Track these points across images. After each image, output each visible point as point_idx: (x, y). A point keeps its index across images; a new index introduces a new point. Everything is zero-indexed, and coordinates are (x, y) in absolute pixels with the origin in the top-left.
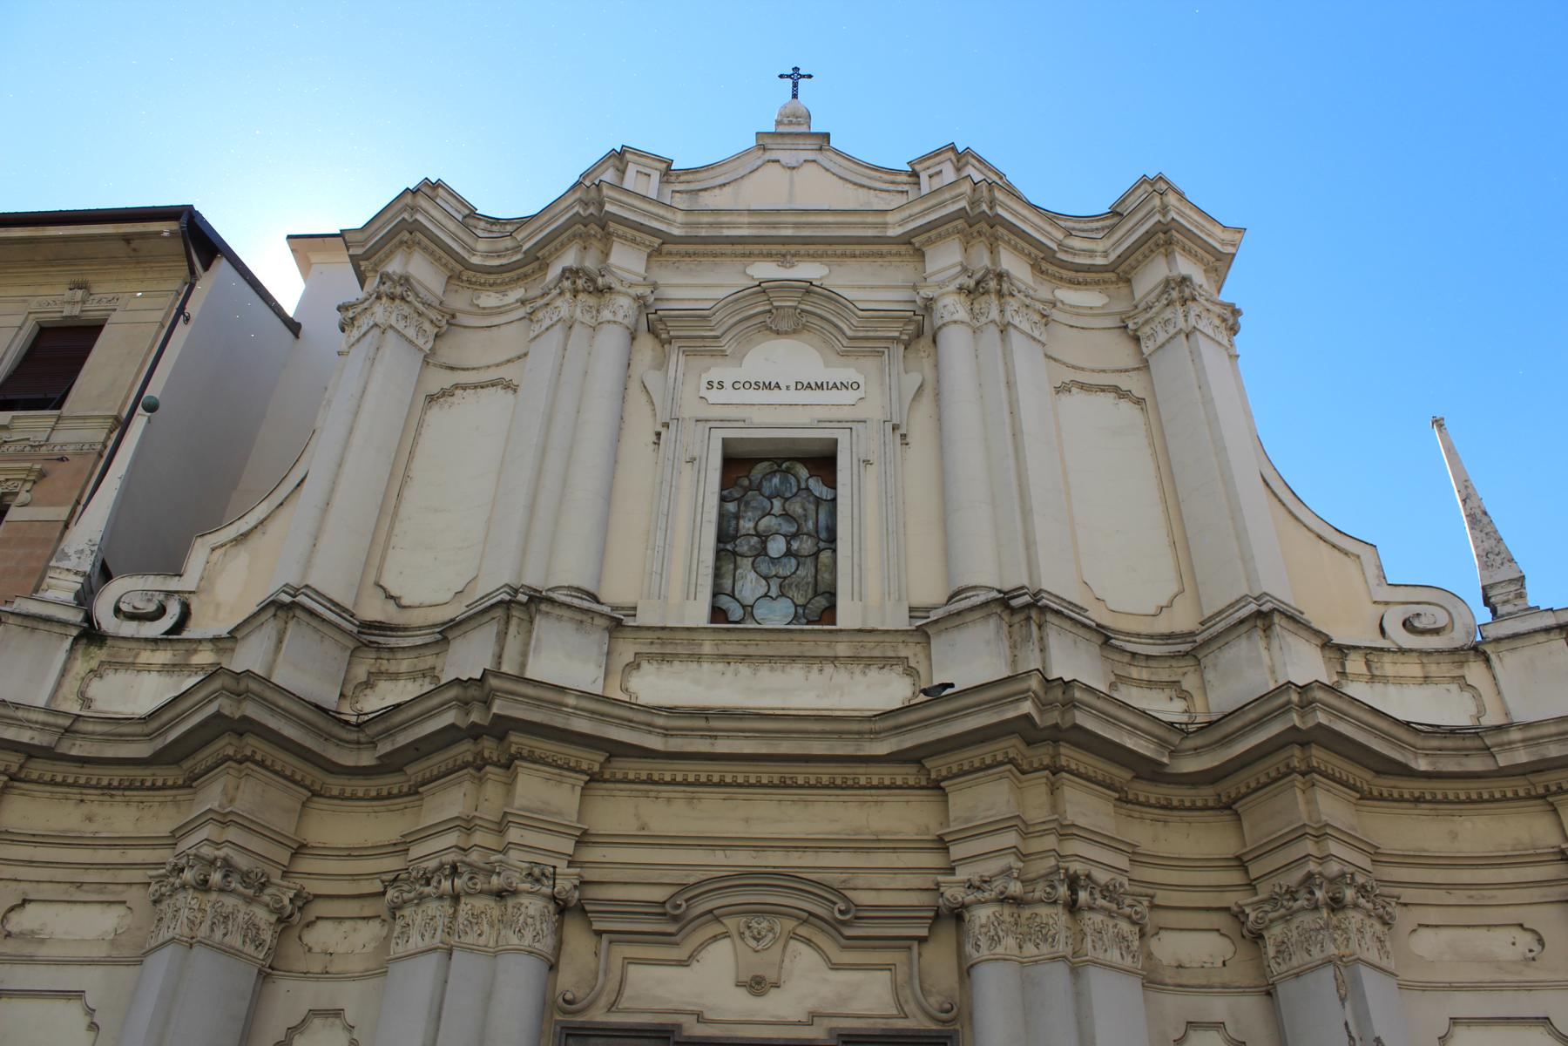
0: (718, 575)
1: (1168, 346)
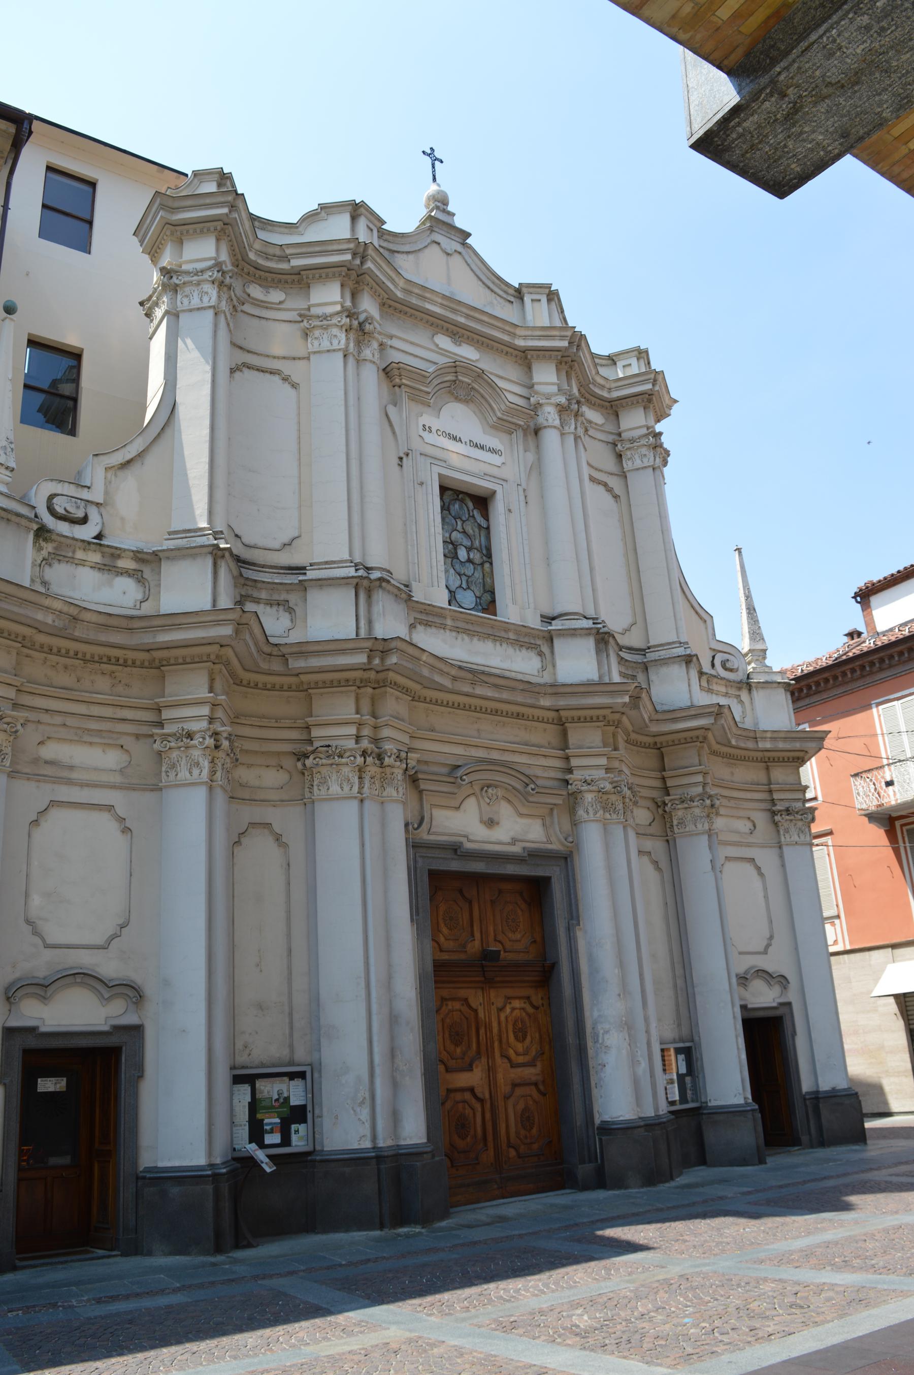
1: (641, 471)
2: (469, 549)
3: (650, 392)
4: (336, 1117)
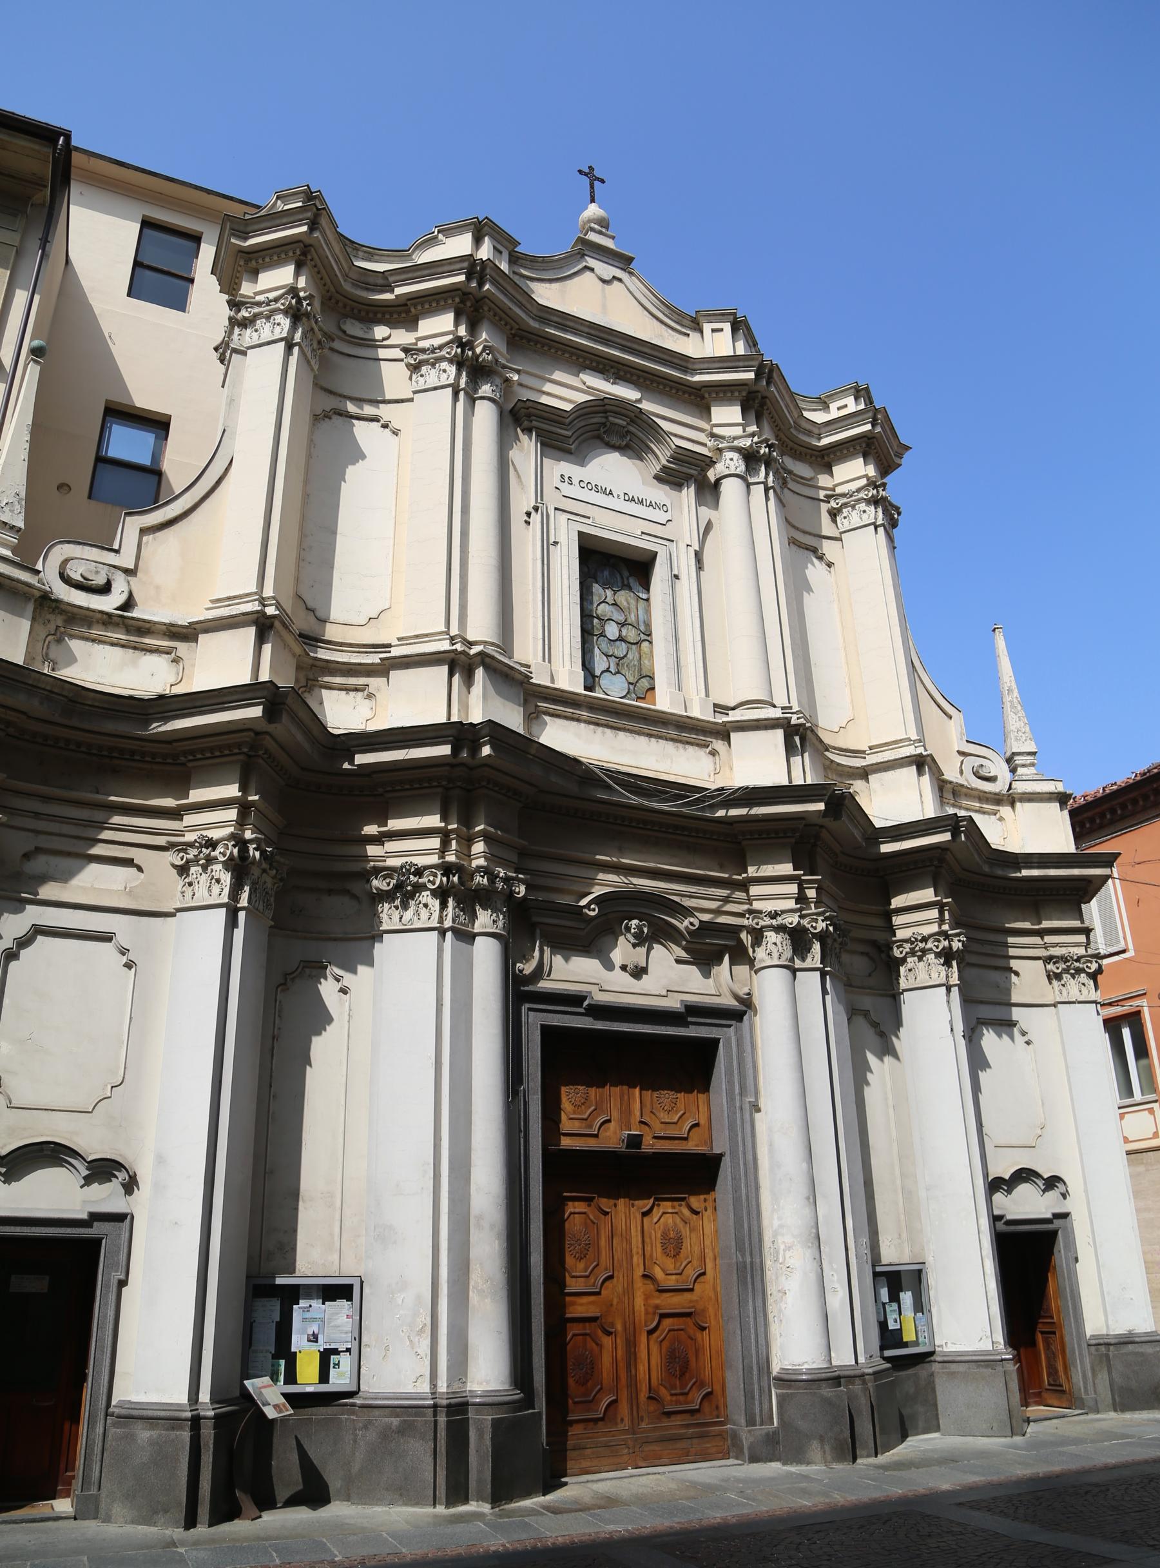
2: (622, 625)
3: (870, 435)
4: (387, 1348)
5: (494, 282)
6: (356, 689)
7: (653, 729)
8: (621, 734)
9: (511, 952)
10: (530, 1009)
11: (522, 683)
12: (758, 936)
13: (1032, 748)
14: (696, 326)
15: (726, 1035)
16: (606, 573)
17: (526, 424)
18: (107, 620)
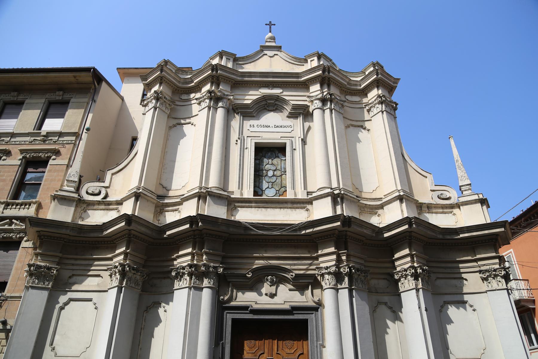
0: (255, 181)
5: (221, 70)
6: (176, 210)
7: (281, 205)
8: (269, 209)
9: (217, 292)
10: (227, 313)
11: (227, 198)
12: (322, 275)
13: (468, 182)
14: (306, 61)
15: (311, 318)
16: (269, 154)
17: (237, 111)
18: (99, 203)
